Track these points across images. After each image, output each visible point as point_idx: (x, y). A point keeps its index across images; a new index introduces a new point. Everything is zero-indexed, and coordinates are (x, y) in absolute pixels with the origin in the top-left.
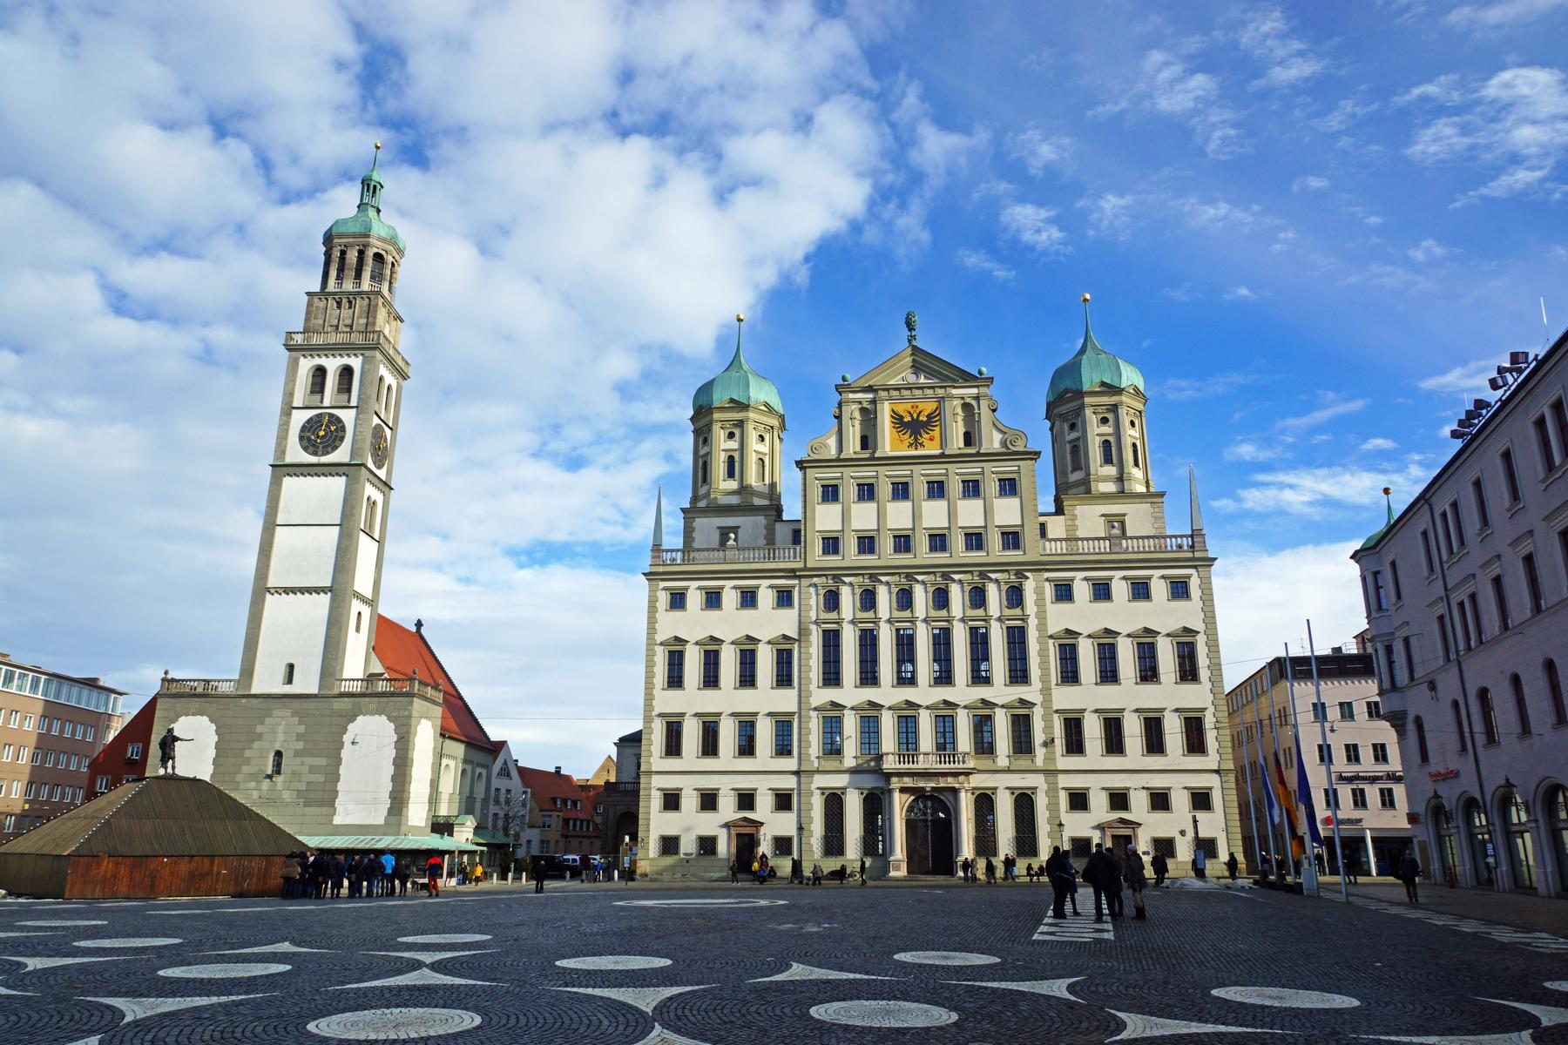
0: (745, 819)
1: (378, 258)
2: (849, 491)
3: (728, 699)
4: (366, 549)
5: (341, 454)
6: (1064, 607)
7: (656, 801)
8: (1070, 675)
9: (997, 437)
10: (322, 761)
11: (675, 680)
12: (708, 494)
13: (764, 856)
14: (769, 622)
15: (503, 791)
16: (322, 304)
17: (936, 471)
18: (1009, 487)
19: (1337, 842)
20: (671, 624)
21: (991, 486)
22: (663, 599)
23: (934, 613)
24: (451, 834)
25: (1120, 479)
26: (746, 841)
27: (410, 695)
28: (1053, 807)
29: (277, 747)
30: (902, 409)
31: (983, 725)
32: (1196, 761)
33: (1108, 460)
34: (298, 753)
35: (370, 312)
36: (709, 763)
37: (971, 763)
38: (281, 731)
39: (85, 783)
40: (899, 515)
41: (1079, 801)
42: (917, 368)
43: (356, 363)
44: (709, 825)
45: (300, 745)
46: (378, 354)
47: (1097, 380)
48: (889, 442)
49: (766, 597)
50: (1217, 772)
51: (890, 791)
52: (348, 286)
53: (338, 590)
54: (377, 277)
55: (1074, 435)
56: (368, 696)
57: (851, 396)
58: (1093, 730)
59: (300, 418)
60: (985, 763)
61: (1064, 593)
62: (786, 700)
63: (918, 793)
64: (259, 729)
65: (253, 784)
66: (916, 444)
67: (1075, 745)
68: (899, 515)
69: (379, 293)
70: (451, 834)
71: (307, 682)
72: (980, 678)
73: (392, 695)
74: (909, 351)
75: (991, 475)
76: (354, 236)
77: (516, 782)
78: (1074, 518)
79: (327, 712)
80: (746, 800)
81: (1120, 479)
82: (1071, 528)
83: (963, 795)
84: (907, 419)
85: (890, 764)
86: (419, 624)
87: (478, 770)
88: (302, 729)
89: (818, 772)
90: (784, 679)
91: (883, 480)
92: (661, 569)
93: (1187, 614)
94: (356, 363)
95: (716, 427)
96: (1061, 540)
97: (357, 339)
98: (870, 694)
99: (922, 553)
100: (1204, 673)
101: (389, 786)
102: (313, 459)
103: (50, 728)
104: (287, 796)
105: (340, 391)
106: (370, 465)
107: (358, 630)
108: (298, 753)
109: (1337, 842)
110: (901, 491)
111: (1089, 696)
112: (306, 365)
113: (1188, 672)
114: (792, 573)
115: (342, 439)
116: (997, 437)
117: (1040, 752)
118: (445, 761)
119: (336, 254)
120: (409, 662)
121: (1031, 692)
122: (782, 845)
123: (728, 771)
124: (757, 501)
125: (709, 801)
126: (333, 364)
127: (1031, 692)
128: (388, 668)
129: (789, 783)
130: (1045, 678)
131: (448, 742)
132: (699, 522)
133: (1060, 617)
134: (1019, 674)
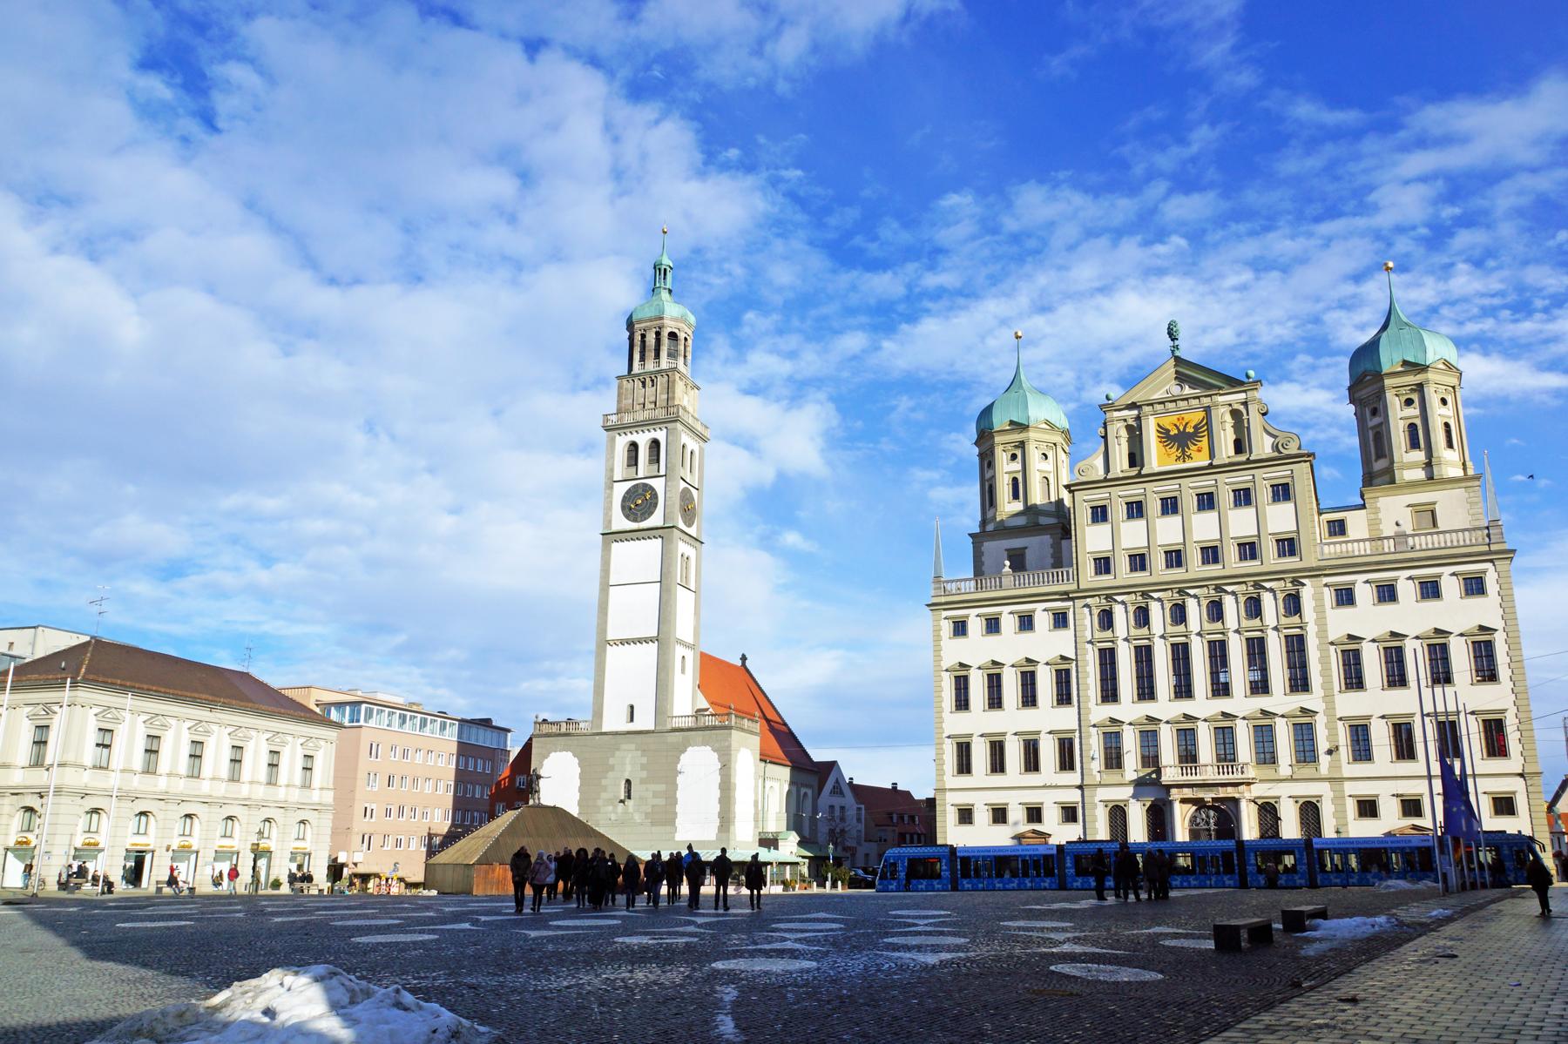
0: (1034, 831)
1: (673, 336)
2: (1118, 511)
3: (1012, 720)
4: (684, 601)
5: (656, 519)
6: (1346, 611)
8: (1354, 679)
9: (1269, 441)
10: (662, 787)
12: (994, 517)
14: (1047, 644)
15: (837, 809)
16: (630, 386)
17: (1205, 483)
18: (1282, 492)
20: (955, 651)
21: (1263, 494)
22: (947, 628)
23: (1208, 626)
24: (776, 848)
25: (1429, 465)
27: (729, 728)
30: (1168, 422)
31: (1225, 737)
32: (1406, 767)
33: (1414, 444)
34: (643, 781)
35: (670, 388)
37: (1251, 773)
39: (487, 808)
40: (1168, 531)
42: (1181, 378)
43: (661, 435)
45: (644, 774)
47: (1398, 359)
48: (1156, 457)
49: (1042, 620)
50: (1521, 775)
51: (1171, 803)
52: (650, 366)
53: (662, 639)
54: (672, 355)
55: (1377, 420)
56: (698, 730)
57: (1116, 414)
58: (1381, 738)
59: (621, 490)
60: (1267, 771)
61: (1345, 597)
62: (1066, 719)
63: (1199, 803)
66: (1184, 456)
67: (1362, 751)
68: (1168, 531)
69: (675, 369)
70: (776, 848)
71: (645, 721)
73: (714, 728)
74: (1172, 362)
75: (1262, 482)
76: (651, 320)
77: (849, 799)
79: (663, 742)
81: (1429, 465)
82: (1374, 523)
83: (1243, 805)
84: (1174, 432)
85: (1171, 774)
86: (744, 658)
87: (803, 790)
88: (644, 760)
89: (1100, 785)
90: (1064, 698)
91: (1152, 497)
92: (943, 600)
93: (1485, 611)
95: (998, 451)
97: (660, 414)
98: (1147, 708)
99: (1195, 567)
100: (1503, 671)
101: (717, 808)
102: (634, 526)
103: (467, 764)
104: (637, 818)
105: (651, 462)
106: (681, 525)
107: (683, 671)
108: (643, 781)
110: (1170, 506)
112: (622, 442)
114: (1066, 596)
115: (656, 505)
116: (1269, 441)
117: (1324, 760)
118: (768, 784)
119: (638, 338)
120: (734, 691)
123: (1016, 788)
124: (1043, 520)
126: (643, 439)
128: (712, 703)
129: (1074, 796)
130: (1327, 685)
131: (770, 766)
132: (989, 546)
133: (1342, 622)
134: (1299, 682)
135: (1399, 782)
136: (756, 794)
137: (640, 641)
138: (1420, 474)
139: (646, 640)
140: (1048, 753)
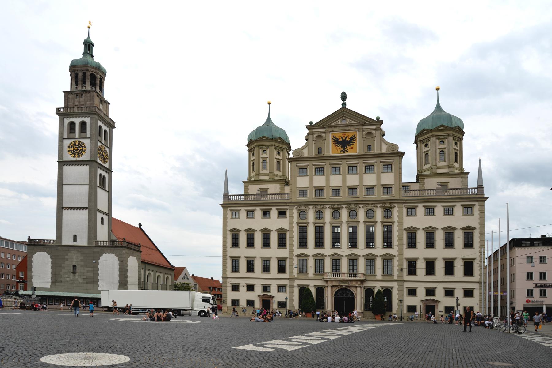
0: (265, 295)
3: (258, 252)
4: (101, 195)
5: (86, 156)
7: (229, 288)
8: (412, 244)
11: (235, 244)
22: (229, 213)
26: (266, 303)
28: (400, 294)
29: (74, 263)
30: (337, 136)
34: (82, 266)
38: (74, 258)
41: (412, 292)
43: (88, 120)
44: (251, 296)
45: (82, 263)
46: (96, 116)
54: (93, 84)
55: (427, 149)
59: (67, 143)
62: (283, 253)
64: (66, 257)
65: (67, 276)
66: (344, 151)
71: (83, 241)
78: (424, 184)
84: (340, 140)
86: (140, 225)
87: (166, 276)
88: (82, 258)
94: (88, 120)
102: (74, 159)
106: (99, 161)
107: (102, 223)
108: (82, 266)
112: (67, 121)
113: (468, 244)
114: (286, 204)
121: (393, 251)
122: (282, 304)
125: (251, 288)
126: (77, 121)
127: (393, 251)
130: (400, 245)
137: (80, 209)
138: (339, 229)
139: (83, 209)
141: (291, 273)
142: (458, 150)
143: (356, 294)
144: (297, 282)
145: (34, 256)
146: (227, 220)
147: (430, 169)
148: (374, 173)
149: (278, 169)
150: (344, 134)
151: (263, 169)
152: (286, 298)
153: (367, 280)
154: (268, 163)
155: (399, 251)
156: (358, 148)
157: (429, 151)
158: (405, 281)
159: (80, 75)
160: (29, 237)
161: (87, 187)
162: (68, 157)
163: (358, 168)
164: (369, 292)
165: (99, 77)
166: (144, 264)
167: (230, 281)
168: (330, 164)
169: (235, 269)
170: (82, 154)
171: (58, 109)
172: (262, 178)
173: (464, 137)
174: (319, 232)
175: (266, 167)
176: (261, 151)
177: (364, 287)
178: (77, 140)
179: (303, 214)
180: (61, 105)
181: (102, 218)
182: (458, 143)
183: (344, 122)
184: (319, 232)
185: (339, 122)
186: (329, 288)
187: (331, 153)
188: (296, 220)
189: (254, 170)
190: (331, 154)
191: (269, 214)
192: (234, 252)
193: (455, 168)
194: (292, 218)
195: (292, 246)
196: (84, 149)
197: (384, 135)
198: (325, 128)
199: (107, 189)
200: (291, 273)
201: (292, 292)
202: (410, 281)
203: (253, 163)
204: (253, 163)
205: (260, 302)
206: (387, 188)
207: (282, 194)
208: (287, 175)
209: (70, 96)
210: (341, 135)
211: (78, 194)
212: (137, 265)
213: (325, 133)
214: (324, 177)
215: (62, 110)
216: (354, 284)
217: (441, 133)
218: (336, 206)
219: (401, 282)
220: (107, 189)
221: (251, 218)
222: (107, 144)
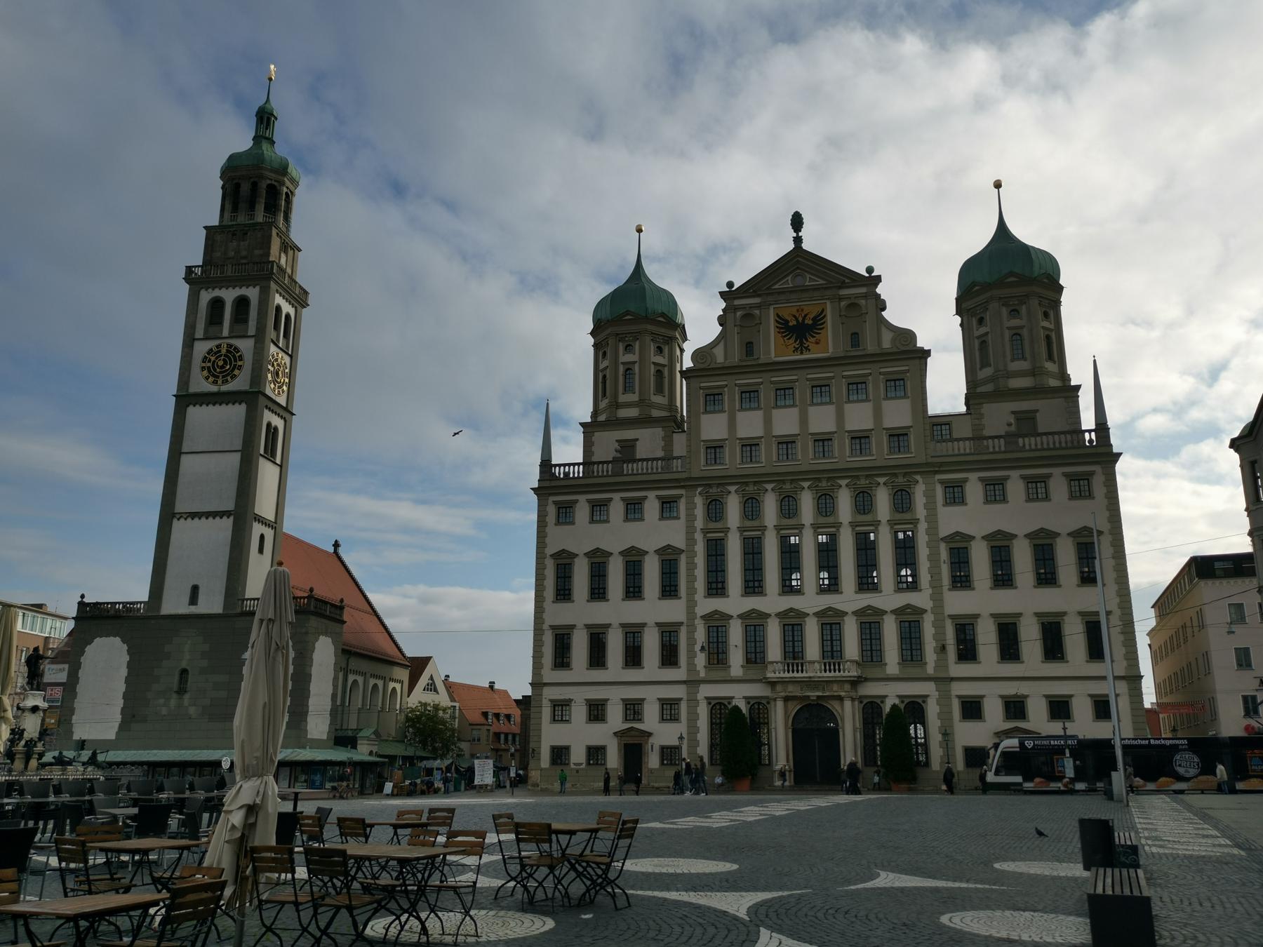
4: (267, 473)
5: (240, 382)
7: (546, 712)
8: (962, 580)
13: (852, 765)
19: (1119, 753)
22: (552, 510)
26: (633, 750)
28: (945, 716)
29: (184, 665)
32: (1095, 669)
36: (598, 675)
41: (972, 709)
43: (253, 293)
53: (241, 513)
55: (983, 330)
58: (987, 637)
59: (201, 348)
62: (673, 611)
65: (162, 701)
66: (802, 348)
67: (967, 652)
71: (212, 603)
72: (866, 583)
80: (633, 709)
86: (336, 545)
87: (372, 682)
90: (669, 589)
94: (253, 293)
96: (968, 439)
98: (753, 603)
102: (214, 389)
104: (192, 710)
107: (261, 550)
109: (1119, 753)
111: (982, 601)
112: (206, 297)
121: (920, 599)
122: (669, 754)
124: (656, 413)
125: (596, 712)
126: (229, 296)
129: (678, 692)
132: (598, 436)
135: (1037, 683)
136: (335, 686)
137: (208, 515)
140: (651, 645)
141: (691, 667)
142: (1051, 330)
143: (843, 720)
144: (706, 691)
145: (88, 649)
146: (547, 530)
147: (992, 379)
148: (867, 400)
149: (659, 390)
150: (800, 310)
151: (625, 391)
152: (681, 738)
153: (866, 680)
154: (637, 377)
155: (932, 597)
156: (830, 342)
157: (987, 334)
158: (953, 679)
159: (245, 188)
160: (83, 596)
161: (239, 455)
162: (201, 384)
163: (833, 390)
164: (871, 709)
165: (285, 190)
166: (349, 655)
167: (550, 694)
168: (772, 382)
169: (562, 658)
170: (234, 377)
171: (189, 270)
172: (624, 413)
173: (1064, 298)
174: (753, 551)
175: (633, 387)
176: (621, 347)
177: (861, 699)
178: (224, 343)
179: (715, 510)
180: (198, 259)
181: (262, 537)
182: (1052, 314)
183: (799, 281)
184: (753, 551)
185: (789, 282)
186: (780, 704)
187: (773, 355)
188: (699, 524)
189: (604, 394)
190: (773, 357)
191: (641, 511)
192: (561, 614)
193: (1048, 374)
194: (691, 518)
195: (692, 591)
196: (240, 363)
197: (884, 309)
198: (759, 296)
199: (278, 461)
200: (691, 667)
201: (693, 718)
202: (969, 679)
203: (604, 377)
204: (604, 377)
205: (619, 750)
206: (898, 436)
207: (668, 458)
208: (678, 404)
209: (218, 238)
210: (794, 311)
211: (210, 474)
212: (332, 660)
213: (759, 306)
214: (760, 413)
215: (198, 271)
216: (836, 690)
217: (1011, 290)
218: (788, 486)
219: (944, 681)
220: (278, 461)
221: (600, 522)
222: (287, 347)
